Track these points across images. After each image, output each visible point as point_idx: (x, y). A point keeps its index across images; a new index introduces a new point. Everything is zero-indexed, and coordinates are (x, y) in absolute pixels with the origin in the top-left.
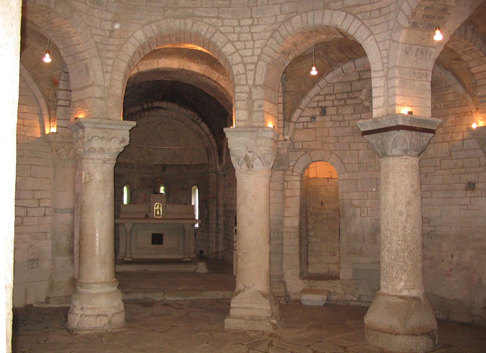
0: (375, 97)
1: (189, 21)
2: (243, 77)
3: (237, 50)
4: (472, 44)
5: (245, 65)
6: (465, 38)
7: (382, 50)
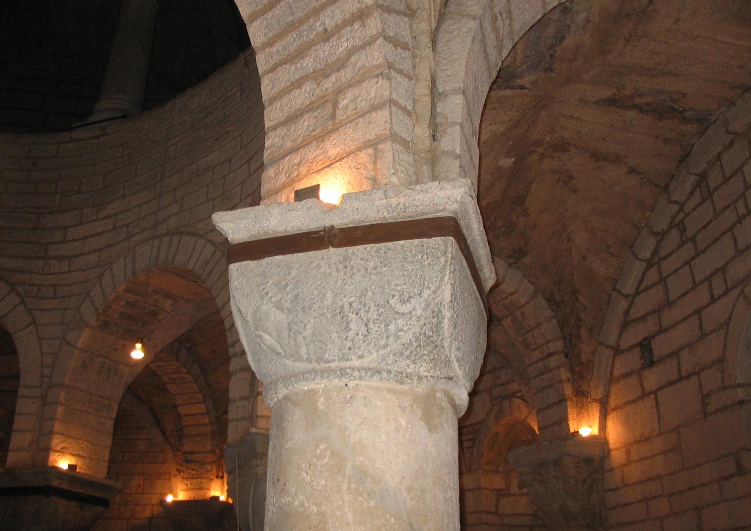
4: (185, 370)
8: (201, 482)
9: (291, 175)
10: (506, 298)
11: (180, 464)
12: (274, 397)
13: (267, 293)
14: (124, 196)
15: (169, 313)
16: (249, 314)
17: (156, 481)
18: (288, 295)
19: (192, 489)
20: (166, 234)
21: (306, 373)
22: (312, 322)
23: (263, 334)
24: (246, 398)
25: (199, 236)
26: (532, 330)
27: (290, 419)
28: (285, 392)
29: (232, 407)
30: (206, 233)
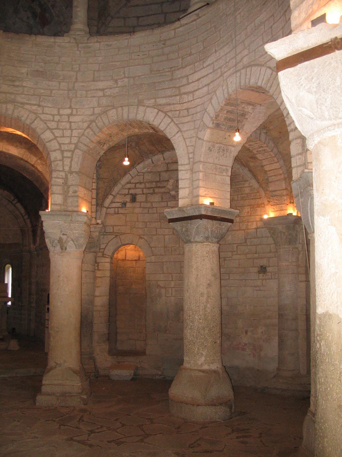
1: (10, 107)
2: (60, 163)
3: (56, 138)
4: (265, 145)
5: (62, 152)
9: (308, 12)
11: (269, 198)
12: (313, 143)
13: (302, 85)
14: (216, 51)
15: (252, 113)
16: (293, 99)
17: (257, 209)
18: (314, 84)
19: (277, 211)
20: (243, 68)
21: (329, 127)
22: (330, 97)
23: (302, 109)
24: (300, 154)
25: (262, 65)
27: (323, 154)
28: (319, 139)
29: (293, 160)
30: (266, 63)
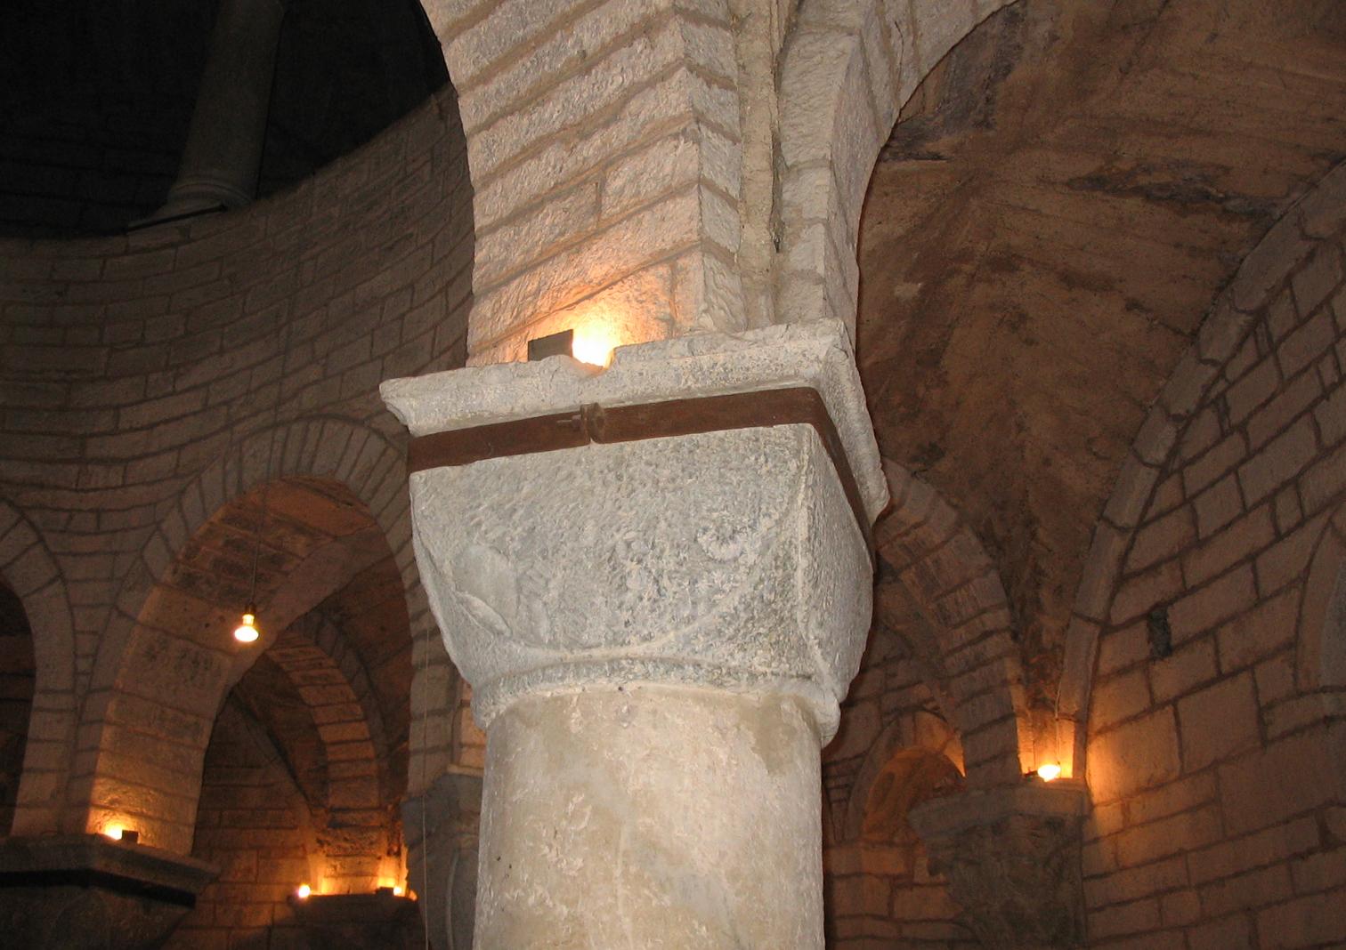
0: (30, 770)
4: (331, 662)
6: (317, 643)
7: (83, 632)
8: (360, 863)
9: (522, 314)
10: (907, 533)
11: (323, 831)
12: (492, 711)
13: (479, 524)
14: (222, 351)
15: (303, 559)
16: (447, 562)
17: (280, 861)
18: (516, 528)
19: (344, 875)
20: (298, 419)
21: (548, 667)
22: (559, 576)
23: (471, 598)
24: (441, 713)
25: (356, 422)
26: (953, 590)
27: (520, 749)
28: (512, 701)
29: (415, 729)
30: (370, 417)
